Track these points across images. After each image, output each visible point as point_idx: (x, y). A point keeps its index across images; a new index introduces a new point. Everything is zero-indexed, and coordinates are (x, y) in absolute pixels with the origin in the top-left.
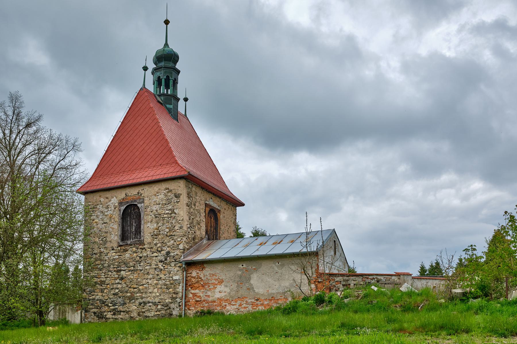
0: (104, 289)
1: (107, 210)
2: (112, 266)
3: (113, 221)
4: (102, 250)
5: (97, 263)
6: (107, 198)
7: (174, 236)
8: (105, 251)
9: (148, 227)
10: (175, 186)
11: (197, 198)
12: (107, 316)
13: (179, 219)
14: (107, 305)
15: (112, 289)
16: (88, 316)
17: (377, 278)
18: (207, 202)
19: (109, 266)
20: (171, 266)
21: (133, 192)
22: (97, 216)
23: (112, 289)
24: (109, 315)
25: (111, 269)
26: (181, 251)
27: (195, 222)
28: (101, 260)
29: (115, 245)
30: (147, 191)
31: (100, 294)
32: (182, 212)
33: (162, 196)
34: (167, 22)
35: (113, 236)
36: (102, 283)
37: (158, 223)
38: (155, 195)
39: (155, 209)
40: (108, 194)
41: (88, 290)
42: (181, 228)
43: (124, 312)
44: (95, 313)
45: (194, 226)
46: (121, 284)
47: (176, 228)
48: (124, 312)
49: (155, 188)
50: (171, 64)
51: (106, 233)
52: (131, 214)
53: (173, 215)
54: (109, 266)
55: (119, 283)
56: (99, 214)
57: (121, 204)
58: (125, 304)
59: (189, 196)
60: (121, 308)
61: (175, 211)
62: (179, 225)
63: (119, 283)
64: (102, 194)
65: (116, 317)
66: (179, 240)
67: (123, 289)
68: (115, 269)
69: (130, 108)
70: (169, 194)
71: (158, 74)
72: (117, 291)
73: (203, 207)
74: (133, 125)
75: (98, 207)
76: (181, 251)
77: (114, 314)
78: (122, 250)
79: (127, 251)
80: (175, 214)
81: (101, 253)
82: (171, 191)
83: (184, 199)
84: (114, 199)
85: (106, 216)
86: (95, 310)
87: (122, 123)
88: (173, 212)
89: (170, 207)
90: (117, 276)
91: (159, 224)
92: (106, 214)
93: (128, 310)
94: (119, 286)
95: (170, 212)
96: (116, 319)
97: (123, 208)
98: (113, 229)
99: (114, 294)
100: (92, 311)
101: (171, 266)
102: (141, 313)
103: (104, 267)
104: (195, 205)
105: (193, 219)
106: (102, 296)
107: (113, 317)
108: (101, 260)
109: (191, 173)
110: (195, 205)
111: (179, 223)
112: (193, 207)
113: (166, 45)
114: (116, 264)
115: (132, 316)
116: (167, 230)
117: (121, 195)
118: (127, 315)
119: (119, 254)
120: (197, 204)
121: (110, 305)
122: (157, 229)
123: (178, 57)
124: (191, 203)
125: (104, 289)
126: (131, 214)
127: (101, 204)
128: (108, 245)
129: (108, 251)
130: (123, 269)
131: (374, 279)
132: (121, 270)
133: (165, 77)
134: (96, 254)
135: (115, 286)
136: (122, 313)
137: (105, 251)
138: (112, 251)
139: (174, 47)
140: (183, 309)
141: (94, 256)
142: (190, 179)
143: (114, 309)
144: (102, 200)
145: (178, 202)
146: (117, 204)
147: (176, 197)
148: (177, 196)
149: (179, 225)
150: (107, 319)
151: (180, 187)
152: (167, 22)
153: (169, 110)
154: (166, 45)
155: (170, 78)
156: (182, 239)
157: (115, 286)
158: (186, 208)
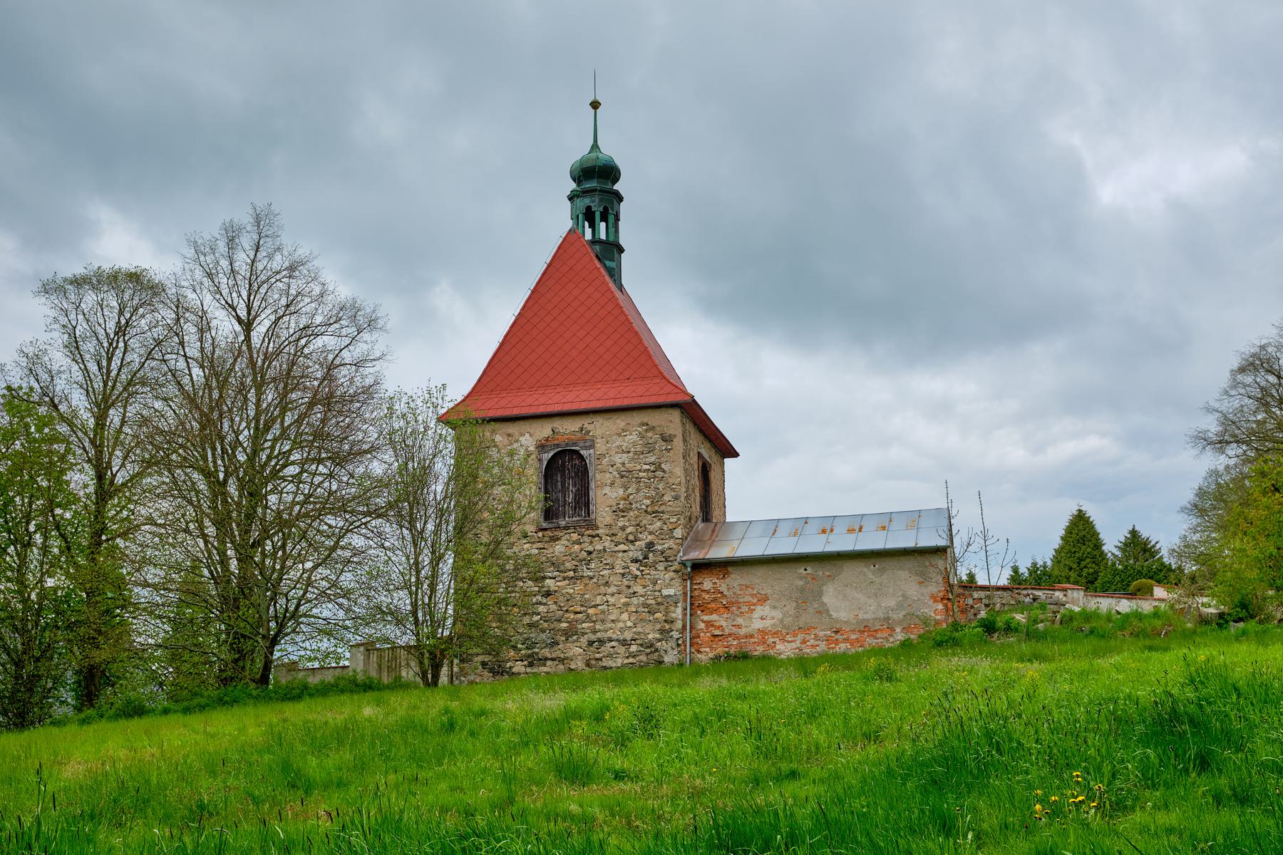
21: (569, 427)
33: (634, 437)
34: (595, 105)
38: (619, 435)
43: (553, 659)
44: (484, 664)
47: (666, 498)
48: (553, 659)
49: (620, 421)
53: (659, 474)
55: (540, 603)
57: (541, 447)
66: (673, 520)
70: (650, 434)
77: (531, 665)
79: (558, 539)
94: (541, 609)
95: (652, 468)
97: (547, 456)
99: (530, 625)
107: (529, 670)
113: (595, 146)
117: (543, 430)
118: (561, 667)
132: (544, 578)
139: (611, 150)
144: (498, 438)
152: (595, 105)
154: (595, 146)
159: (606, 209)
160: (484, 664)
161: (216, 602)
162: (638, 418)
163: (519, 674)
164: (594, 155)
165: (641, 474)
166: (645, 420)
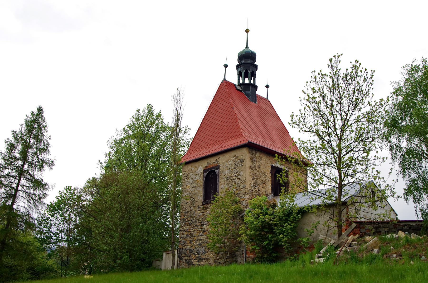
0: (193, 240)
1: (195, 177)
2: (198, 222)
3: (199, 185)
4: (192, 208)
5: (188, 219)
6: (196, 167)
7: (239, 194)
8: (194, 210)
9: (222, 187)
10: (238, 153)
11: (262, 161)
12: (194, 263)
13: (242, 179)
14: (194, 254)
15: (197, 240)
16: (182, 263)
17: (409, 225)
18: (273, 165)
19: (196, 221)
20: (237, 220)
21: (212, 161)
22: (189, 182)
23: (197, 240)
24: (195, 262)
25: (197, 224)
26: (244, 206)
27: (259, 181)
28: (191, 217)
29: (200, 204)
30: (222, 160)
31: (190, 245)
32: (247, 175)
33: (231, 162)
34: (247, 31)
35: (199, 197)
36: (191, 235)
37: (228, 184)
38: (227, 162)
39: (227, 173)
40: (197, 164)
41: (182, 241)
42: (244, 187)
43: (204, 259)
44: (186, 260)
45: (258, 185)
46: (203, 236)
47: (241, 187)
48: (204, 259)
49: (227, 156)
50: (249, 61)
51: (195, 195)
52: (211, 179)
53: (239, 177)
54: (196, 221)
55: (202, 235)
56: (190, 180)
57: (204, 171)
58: (205, 252)
59: (252, 160)
60: (203, 256)
61: (240, 173)
62: (243, 185)
63: (202, 235)
64: (192, 164)
65: (199, 264)
66: (243, 197)
67: (205, 240)
68: (200, 224)
69: (214, 97)
70: (236, 160)
71: (239, 69)
72: (201, 242)
73: (270, 169)
74: (215, 109)
75: (190, 174)
76: (244, 206)
77: (198, 261)
78: (205, 208)
79: (208, 208)
80: (240, 176)
81: (191, 211)
82: (237, 157)
83: (248, 163)
84: (201, 167)
85: (195, 181)
86: (186, 258)
87: (209, 109)
88: (239, 175)
89: (237, 171)
90: (200, 229)
91: (230, 185)
92: (195, 180)
93: (207, 258)
94: (202, 238)
95: (237, 175)
96: (199, 265)
97: (206, 174)
98: (199, 191)
99: (199, 245)
100: (184, 258)
101: (237, 220)
102: (216, 261)
103: (192, 223)
104: (259, 168)
105: (257, 179)
106: (191, 246)
107: (198, 263)
108: (191, 217)
109: (250, 141)
110: (259, 168)
111: (243, 183)
112: (257, 169)
113: (247, 47)
114: (201, 219)
115: (210, 263)
116: (235, 190)
117: (204, 164)
118: (207, 262)
119: (202, 211)
120: (261, 167)
121: (196, 253)
122: (228, 190)
123: (255, 55)
124: (255, 166)
125: (193, 240)
126: (211, 179)
127: (192, 172)
128: (196, 204)
129: (195, 210)
130: (205, 223)
131: (406, 225)
132: (203, 225)
133: (244, 71)
134: (187, 212)
135: (199, 238)
136: (203, 260)
137: (194, 210)
138: (198, 209)
139: (252, 48)
140: (245, 256)
141: (187, 214)
142: (251, 147)
143: (198, 257)
144: (193, 169)
145: (242, 166)
146: (202, 172)
147: (241, 162)
148: (242, 161)
149: (243, 185)
150: (194, 265)
151: (245, 153)
152: (247, 31)
153: (248, 95)
154: (247, 47)
155: (249, 71)
156: (244, 196)
157: (199, 238)
158: (248, 171)
159: (246, 71)
160: (186, 260)
161: (290, 187)
162: (233, 153)
163: (195, 265)
164: (247, 50)
165: (234, 178)
166: (235, 154)
